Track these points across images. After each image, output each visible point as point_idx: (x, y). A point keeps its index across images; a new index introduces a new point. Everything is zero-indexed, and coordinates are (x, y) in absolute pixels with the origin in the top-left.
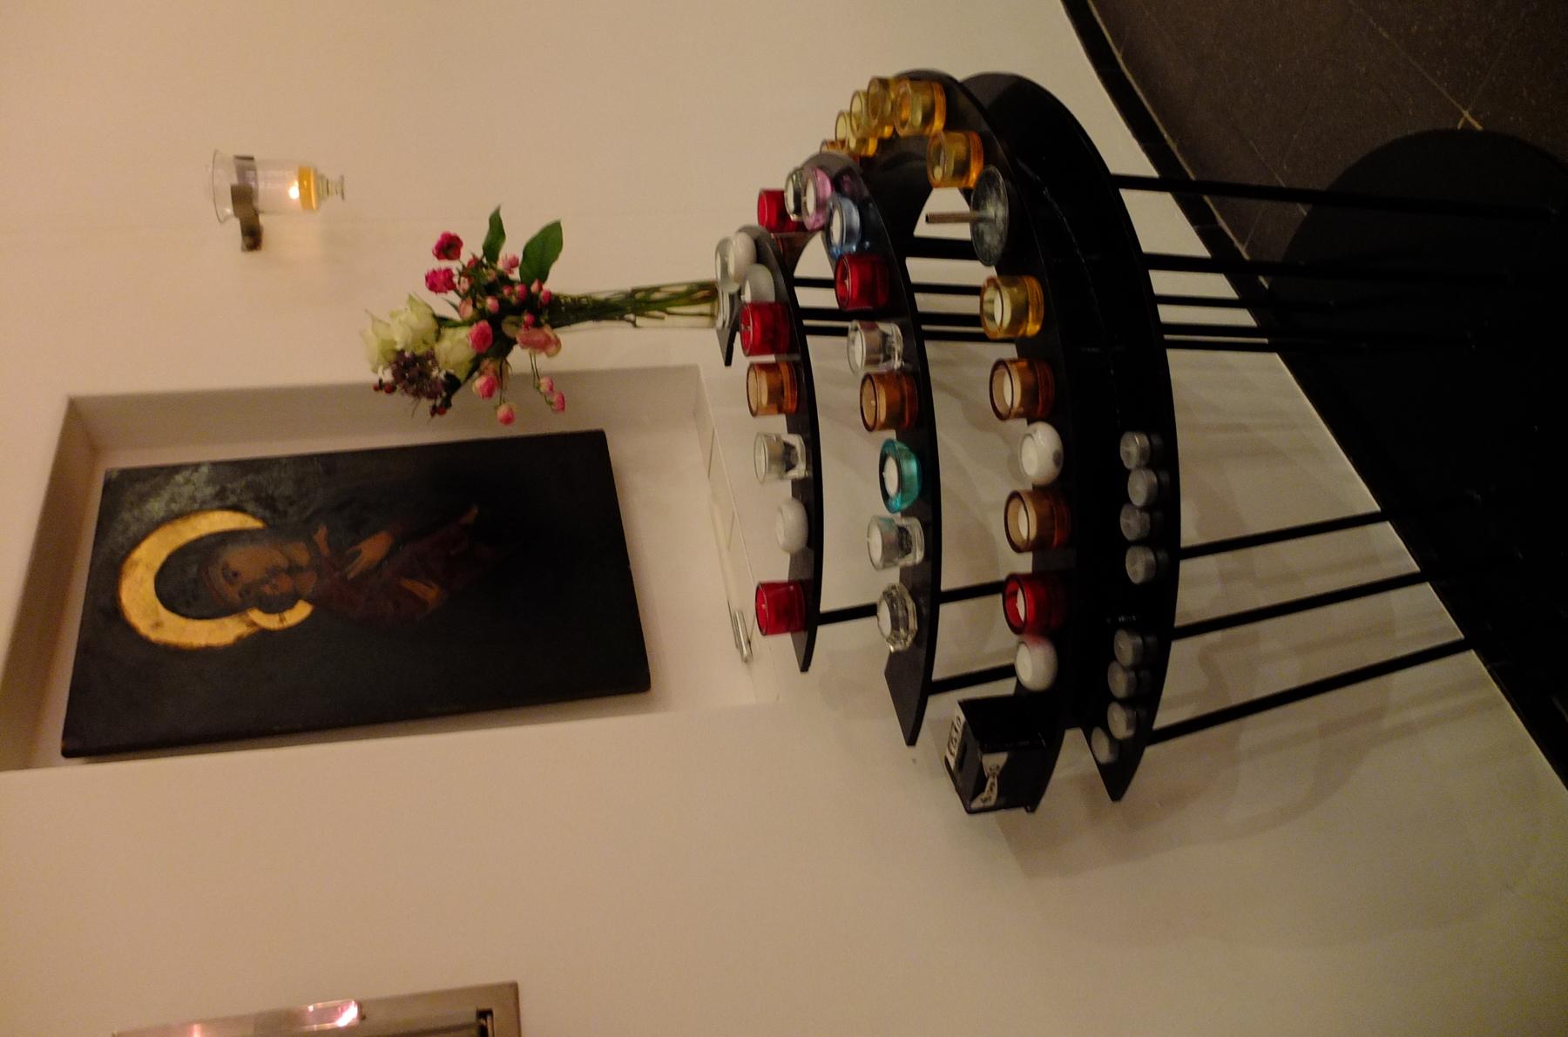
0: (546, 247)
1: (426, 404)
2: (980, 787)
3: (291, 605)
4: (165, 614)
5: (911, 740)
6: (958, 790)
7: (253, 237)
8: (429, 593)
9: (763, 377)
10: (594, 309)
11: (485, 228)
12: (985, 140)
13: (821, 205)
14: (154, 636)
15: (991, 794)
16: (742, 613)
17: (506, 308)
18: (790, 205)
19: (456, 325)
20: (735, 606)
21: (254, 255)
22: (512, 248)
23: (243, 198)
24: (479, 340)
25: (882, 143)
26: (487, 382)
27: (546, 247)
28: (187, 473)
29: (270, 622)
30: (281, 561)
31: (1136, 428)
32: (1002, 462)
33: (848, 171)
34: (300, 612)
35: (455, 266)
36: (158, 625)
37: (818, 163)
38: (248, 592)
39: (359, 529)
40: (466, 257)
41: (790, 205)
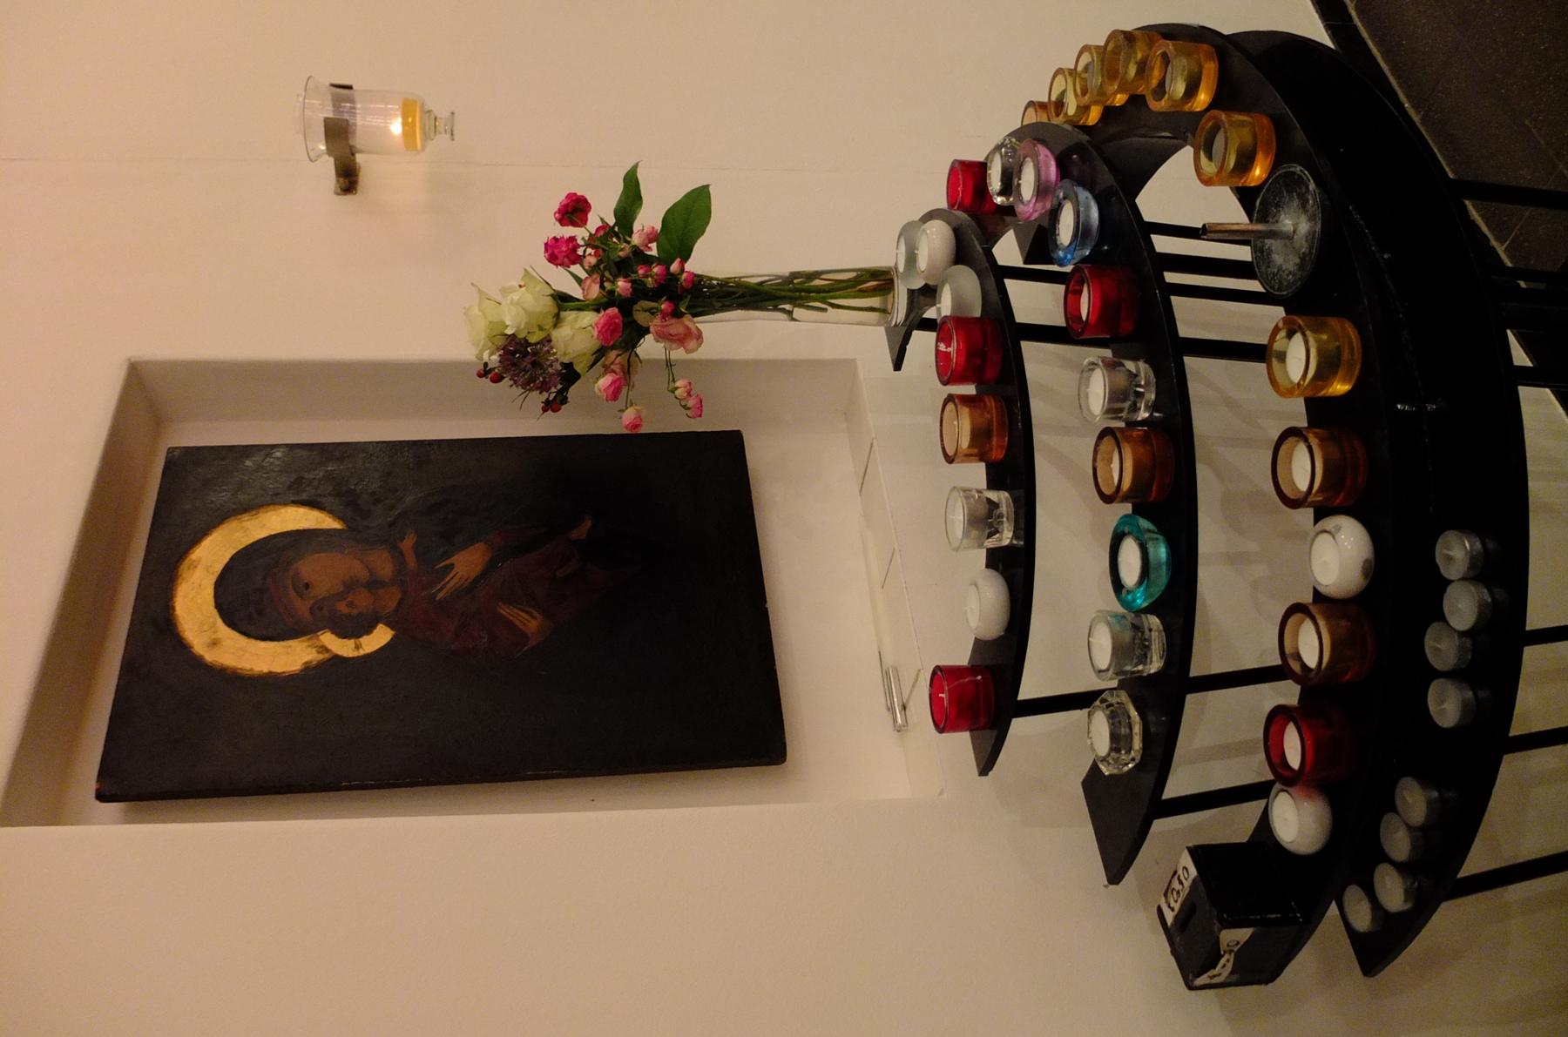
0: (690, 216)
1: (537, 398)
2: (1213, 960)
3: (368, 629)
4: (224, 631)
5: (1115, 874)
6: (1174, 952)
7: (348, 178)
8: (530, 623)
9: (965, 412)
10: (743, 296)
11: (619, 188)
12: (1278, 123)
13: (1042, 190)
14: (210, 657)
15: (1224, 967)
16: (896, 669)
17: (640, 292)
18: (995, 183)
19: (581, 306)
20: (889, 659)
21: (348, 199)
22: (649, 219)
23: (338, 133)
24: (607, 330)
25: (1109, 113)
26: (613, 382)
27: (690, 216)
28: (258, 458)
29: (344, 648)
30: (363, 575)
31: (1464, 525)
32: (1284, 567)
33: (1078, 147)
34: (380, 637)
35: (581, 234)
36: (214, 643)
37: (1030, 135)
38: (321, 609)
39: (452, 538)
40: (593, 223)
41: (995, 183)
